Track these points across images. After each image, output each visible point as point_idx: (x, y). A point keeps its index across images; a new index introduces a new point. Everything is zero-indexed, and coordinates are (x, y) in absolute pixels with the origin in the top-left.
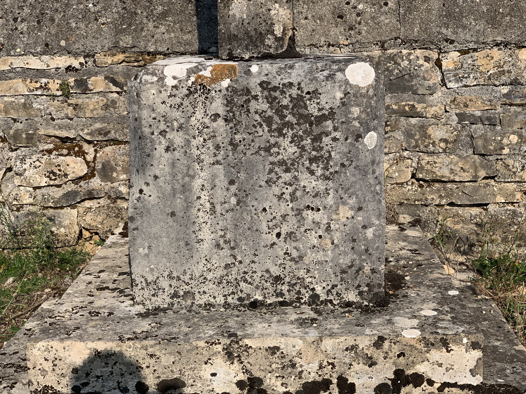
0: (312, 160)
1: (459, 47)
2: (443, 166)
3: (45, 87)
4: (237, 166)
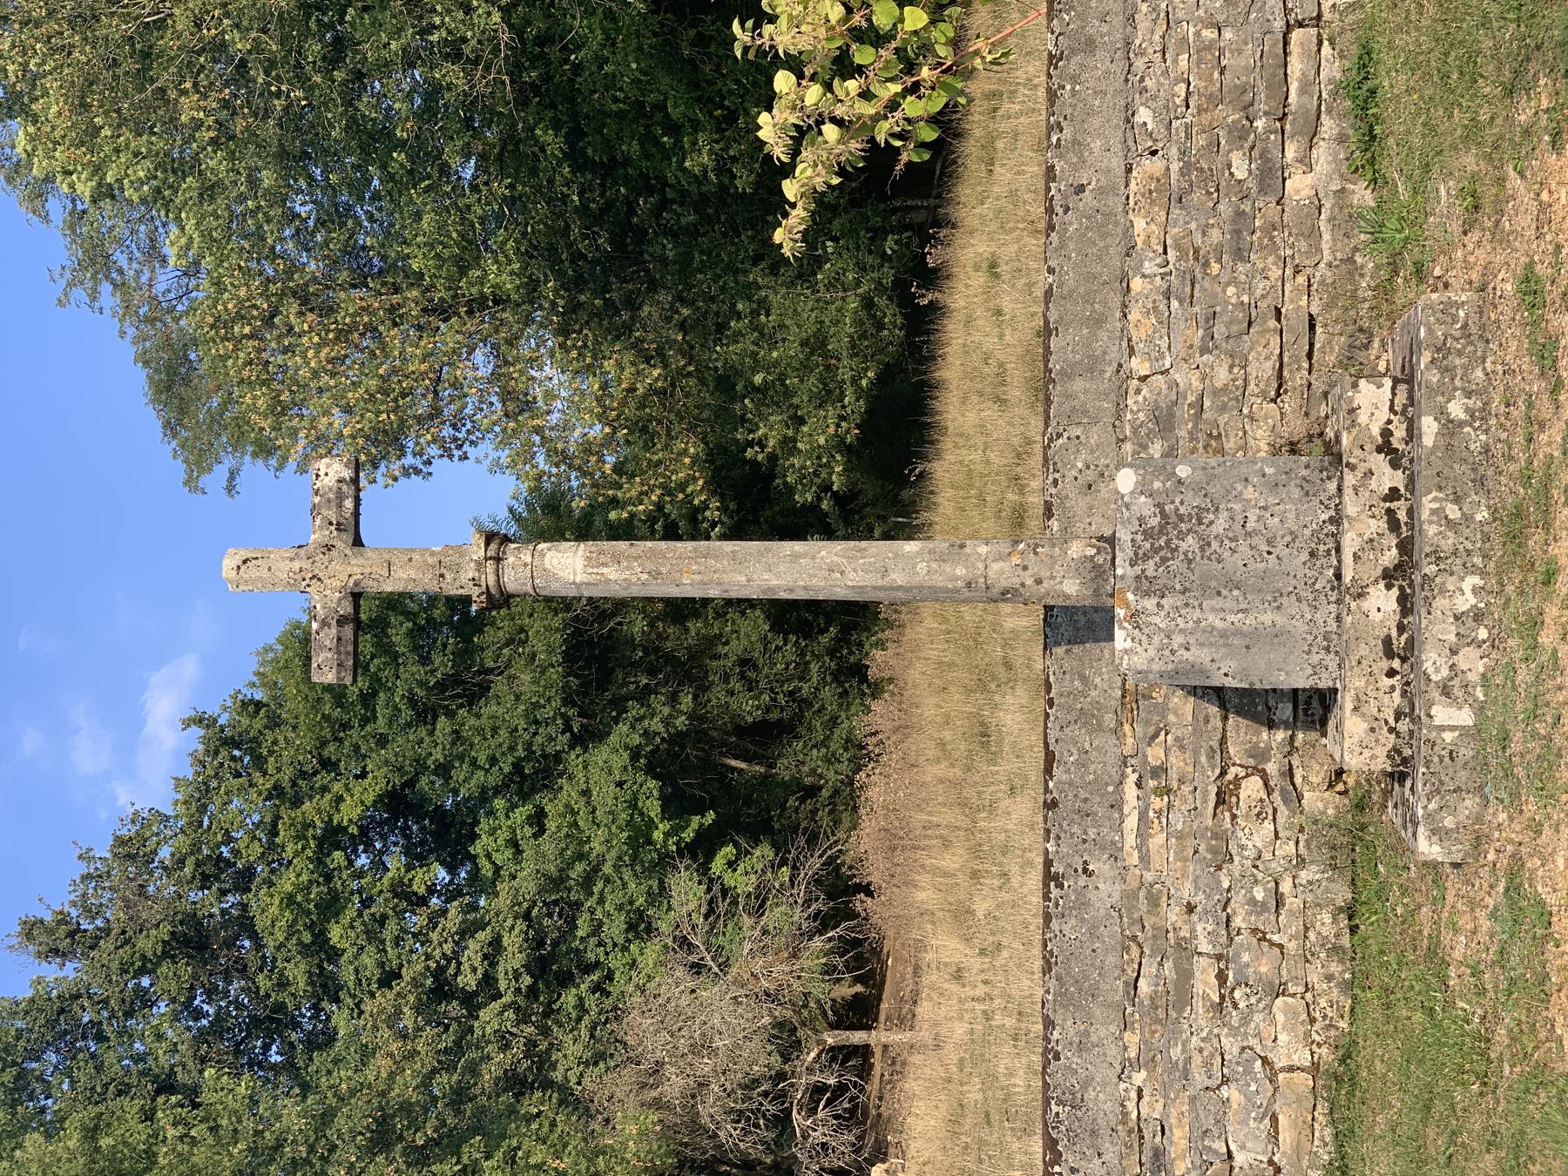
0: (1200, 523)
1: (1126, 357)
2: (1262, 369)
3: (1159, 813)
4: (1204, 589)
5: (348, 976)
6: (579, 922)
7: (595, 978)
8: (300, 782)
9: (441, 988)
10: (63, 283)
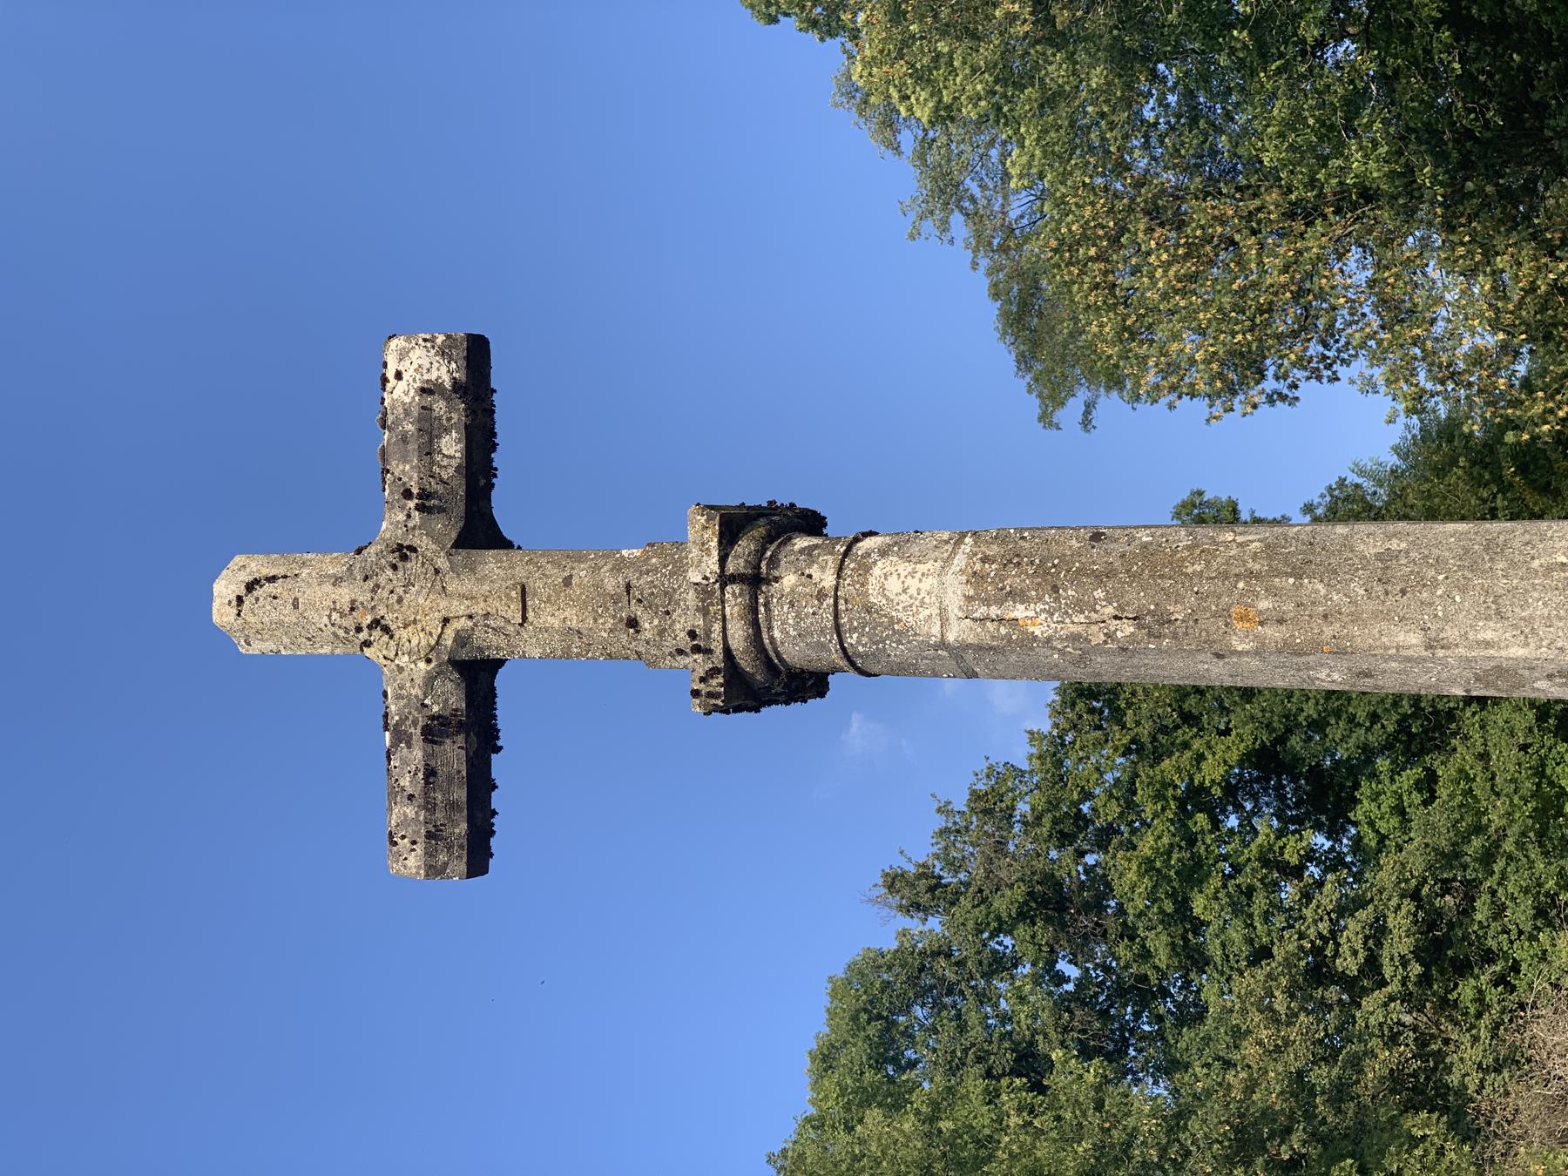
5: (1214, 950)
6: (1477, 904)
7: (1498, 968)
8: (1160, 737)
9: (1319, 971)
10: (913, 216)
